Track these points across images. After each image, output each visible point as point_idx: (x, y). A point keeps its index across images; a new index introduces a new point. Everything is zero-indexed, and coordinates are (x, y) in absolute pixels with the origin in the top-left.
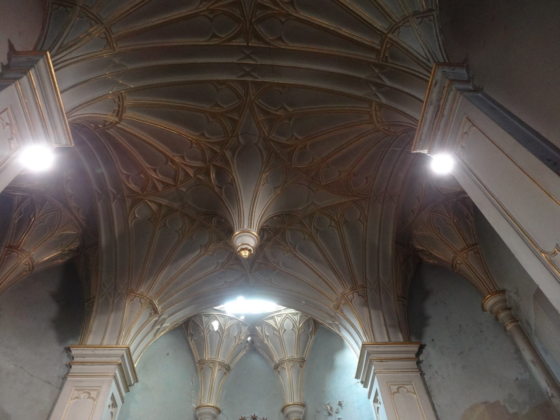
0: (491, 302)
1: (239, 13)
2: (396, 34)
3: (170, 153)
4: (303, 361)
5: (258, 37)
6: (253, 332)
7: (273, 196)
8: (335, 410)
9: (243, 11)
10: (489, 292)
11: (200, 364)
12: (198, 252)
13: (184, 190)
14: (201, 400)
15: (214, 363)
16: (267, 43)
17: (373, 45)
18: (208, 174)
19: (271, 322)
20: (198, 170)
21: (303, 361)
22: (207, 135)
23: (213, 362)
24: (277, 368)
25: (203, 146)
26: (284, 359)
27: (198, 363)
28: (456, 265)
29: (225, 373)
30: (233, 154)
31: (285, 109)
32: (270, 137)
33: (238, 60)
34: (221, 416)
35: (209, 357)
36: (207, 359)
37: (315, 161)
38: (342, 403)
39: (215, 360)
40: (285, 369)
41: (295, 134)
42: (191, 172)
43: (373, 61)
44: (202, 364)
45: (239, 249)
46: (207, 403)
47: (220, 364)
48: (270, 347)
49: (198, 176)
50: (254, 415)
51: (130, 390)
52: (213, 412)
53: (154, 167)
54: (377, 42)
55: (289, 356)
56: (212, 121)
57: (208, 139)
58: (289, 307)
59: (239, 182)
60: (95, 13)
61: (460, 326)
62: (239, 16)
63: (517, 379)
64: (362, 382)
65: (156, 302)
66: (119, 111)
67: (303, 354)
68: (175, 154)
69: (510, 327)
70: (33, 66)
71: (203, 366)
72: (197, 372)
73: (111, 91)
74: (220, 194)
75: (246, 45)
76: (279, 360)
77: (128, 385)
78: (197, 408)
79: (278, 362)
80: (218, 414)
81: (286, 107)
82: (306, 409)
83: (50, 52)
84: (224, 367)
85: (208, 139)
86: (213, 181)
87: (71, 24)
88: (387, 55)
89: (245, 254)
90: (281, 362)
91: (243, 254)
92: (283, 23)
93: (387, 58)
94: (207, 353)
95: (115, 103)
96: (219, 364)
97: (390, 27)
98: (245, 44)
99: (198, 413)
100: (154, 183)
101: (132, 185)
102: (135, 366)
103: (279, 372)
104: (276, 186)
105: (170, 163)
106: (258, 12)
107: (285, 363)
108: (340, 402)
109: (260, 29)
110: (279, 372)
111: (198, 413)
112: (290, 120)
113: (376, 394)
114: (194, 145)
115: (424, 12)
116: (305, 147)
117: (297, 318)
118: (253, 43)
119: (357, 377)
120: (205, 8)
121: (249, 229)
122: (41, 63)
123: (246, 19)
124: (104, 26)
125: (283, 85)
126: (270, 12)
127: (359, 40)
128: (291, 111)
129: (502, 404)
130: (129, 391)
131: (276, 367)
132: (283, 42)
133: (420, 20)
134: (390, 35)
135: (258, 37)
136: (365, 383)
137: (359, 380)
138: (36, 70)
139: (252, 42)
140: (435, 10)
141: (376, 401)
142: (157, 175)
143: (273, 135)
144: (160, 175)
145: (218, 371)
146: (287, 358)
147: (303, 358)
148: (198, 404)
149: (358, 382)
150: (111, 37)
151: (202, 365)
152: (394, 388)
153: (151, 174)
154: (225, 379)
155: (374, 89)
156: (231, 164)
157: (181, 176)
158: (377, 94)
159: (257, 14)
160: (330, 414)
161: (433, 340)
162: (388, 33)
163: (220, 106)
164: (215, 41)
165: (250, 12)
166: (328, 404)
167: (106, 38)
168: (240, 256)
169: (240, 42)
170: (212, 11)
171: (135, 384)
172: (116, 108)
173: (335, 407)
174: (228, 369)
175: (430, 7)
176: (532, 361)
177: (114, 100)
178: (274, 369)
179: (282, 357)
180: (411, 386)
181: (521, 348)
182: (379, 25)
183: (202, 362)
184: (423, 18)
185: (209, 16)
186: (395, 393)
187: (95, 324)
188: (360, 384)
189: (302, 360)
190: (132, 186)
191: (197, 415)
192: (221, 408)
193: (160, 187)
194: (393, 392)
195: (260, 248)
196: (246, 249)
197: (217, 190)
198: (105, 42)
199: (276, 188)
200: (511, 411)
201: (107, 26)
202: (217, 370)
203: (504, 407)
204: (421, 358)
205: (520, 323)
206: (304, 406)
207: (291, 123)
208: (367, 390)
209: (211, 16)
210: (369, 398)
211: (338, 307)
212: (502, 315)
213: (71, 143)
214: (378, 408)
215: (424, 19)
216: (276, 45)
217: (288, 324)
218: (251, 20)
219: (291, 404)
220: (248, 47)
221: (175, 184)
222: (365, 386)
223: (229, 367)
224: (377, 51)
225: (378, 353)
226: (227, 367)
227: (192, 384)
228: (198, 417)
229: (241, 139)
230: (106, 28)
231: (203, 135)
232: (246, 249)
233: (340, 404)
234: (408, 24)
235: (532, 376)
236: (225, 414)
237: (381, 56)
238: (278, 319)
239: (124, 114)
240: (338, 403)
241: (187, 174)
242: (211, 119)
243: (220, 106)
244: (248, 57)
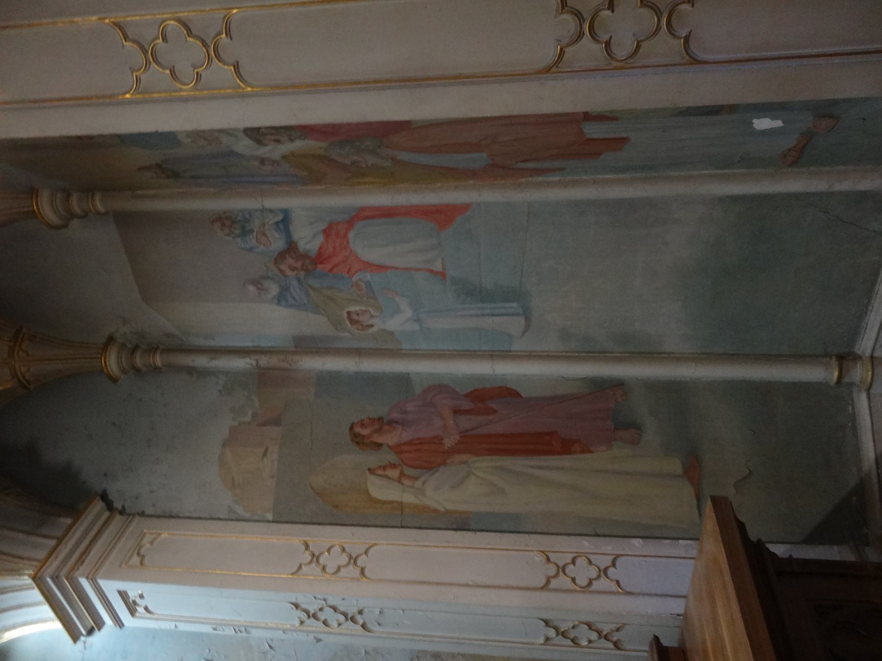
0: (112, 362)
10: (98, 358)
28: (24, 377)
61: (114, 424)
63: (220, 391)
69: (158, 361)
129: (236, 424)
152: (136, 560)
161: (105, 475)
176: (212, 359)
180: (147, 535)
181: (191, 364)
186: (142, 563)
194: (138, 563)
200: (248, 418)
203: (240, 424)
204: (118, 505)
205: (161, 347)
212: (139, 360)
214: (146, 609)
222: (99, 624)
225: (64, 563)
235: (227, 373)
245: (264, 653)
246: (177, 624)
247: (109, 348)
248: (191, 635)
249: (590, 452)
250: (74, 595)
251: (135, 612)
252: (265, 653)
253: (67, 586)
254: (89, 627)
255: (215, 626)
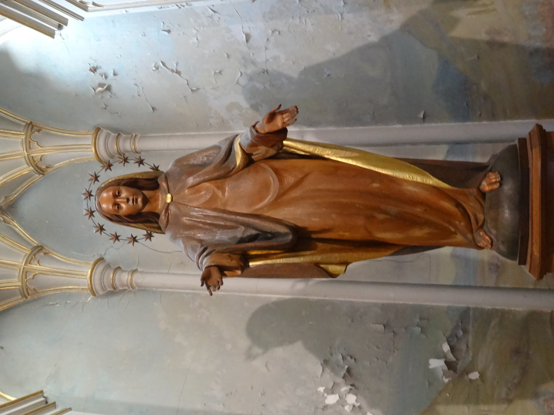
4: (31, 126)
8: (102, 80)
11: (28, 294)
14: (83, 289)
15: (27, 272)
21: (31, 127)
23: (25, 272)
24: (41, 169)
26: (26, 155)
27: (27, 298)
29: (45, 254)
34: (107, 258)
35: (16, 280)
36: (20, 284)
38: (93, 67)
39: (22, 270)
40: (42, 155)
44: (27, 290)
46: (86, 279)
47: (29, 261)
48: (5, 180)
50: (84, 194)
51: (53, 401)
52: (100, 268)
55: (21, 149)
64: (60, 27)
67: (20, 125)
71: (30, 289)
72: (39, 299)
76: (29, 165)
77: (44, 405)
78: (94, 294)
79: (31, 168)
80: (105, 261)
82: (104, 128)
84: (34, 255)
90: (31, 161)
94: (10, 284)
96: (30, 263)
99: (101, 293)
102: (13, 399)
103: (47, 167)
107: (32, 155)
108: (91, 70)
110: (47, 167)
111: (101, 293)
119: (51, 34)
130: (54, 403)
131: (41, 171)
137: (57, 32)
145: (40, 265)
146: (25, 152)
147: (26, 125)
148: (89, 293)
149: (61, 35)
151: (29, 290)
154: (55, 253)
160: (109, 89)
166: (95, 90)
171: (45, 395)
173: (97, 78)
174: (39, 248)
178: (44, 175)
179: (23, 160)
183: (25, 292)
187: (452, 360)
188: (62, 31)
189: (28, 127)
191: (104, 293)
192: (97, 257)
202: (38, 266)
206: (98, 130)
208: (71, 19)
210: (82, 19)
214: (94, 4)
219: (93, 149)
222: (65, 22)
223: (38, 247)
226: (36, 251)
227: (58, 305)
228: (106, 291)
233: (93, 69)
236: (105, 252)
240: (92, 73)
245: (210, 17)
246: (127, 10)
247: (100, 262)
248: (143, 15)
249: (164, 233)
250: (31, 9)
251: (87, 8)
252: (211, 17)
253: (18, 4)
254: (58, 25)
255: (160, 6)
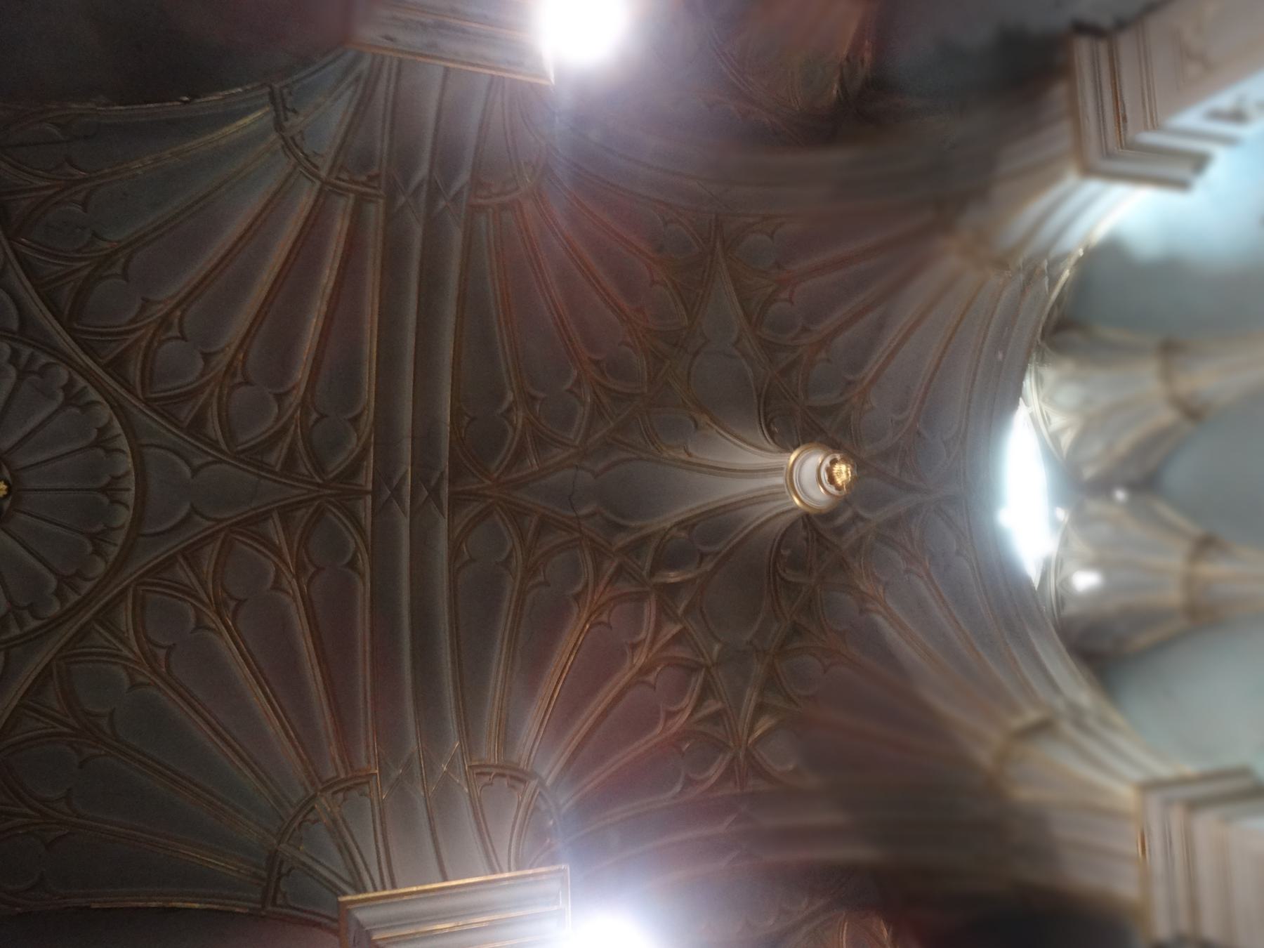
1: (304, 510)
2: (318, 161)
3: (623, 676)
5: (354, 470)
6: (1101, 487)
7: (717, 431)
9: (300, 502)
12: (879, 619)
13: (717, 647)
16: (365, 450)
17: (349, 210)
18: (673, 589)
19: (1067, 440)
20: (664, 612)
22: (579, 588)
23: (1189, 582)
25: (604, 599)
30: (620, 528)
31: (509, 410)
32: (577, 443)
33: (406, 516)
37: (629, 339)
41: (568, 385)
42: (672, 629)
43: (381, 209)
45: (832, 489)
49: (680, 611)
53: (662, 715)
54: (342, 202)
56: (545, 576)
57: (586, 585)
58: (1018, 392)
59: (682, 511)
60: (292, 811)
62: (311, 510)
65: (1016, 723)
66: (512, 777)
68: (628, 664)
70: (368, 933)
73: (463, 788)
74: (720, 556)
75: (370, 497)
81: (505, 405)
83: (345, 894)
85: (586, 585)
86: (689, 576)
87: (309, 862)
88: (364, 178)
89: (843, 472)
91: (844, 477)
92: (322, 416)
93: (371, 178)
95: (492, 784)
97: (307, 177)
98: (369, 498)
100: (700, 721)
101: (712, 771)
104: (693, 426)
105: (651, 678)
106: (304, 471)
109: (338, 463)
112: (534, 398)
113: (1216, 115)
114: (604, 618)
115: (276, 110)
116: (596, 363)
117: (1049, 374)
118: (366, 480)
119: (1182, 185)
120: (294, 582)
121: (784, 472)
122: (363, 915)
123: (314, 495)
124: (319, 793)
125: (456, 414)
126: (300, 444)
127: (342, 244)
128: (514, 396)
132: (361, 414)
133: (290, 114)
134: (323, 174)
135: (354, 470)
136: (1199, 162)
138: (375, 930)
139: (363, 484)
140: (271, 87)
141: (1237, 116)
142: (682, 710)
143: (572, 437)
144: (683, 704)
150: (346, 780)
153: (678, 725)
155: (442, 203)
156: (644, 532)
157: (680, 652)
158: (452, 193)
159: (307, 473)
162: (319, 178)
163: (510, 556)
164: (364, 563)
165: (302, 488)
167: (349, 789)
168: (849, 486)
169: (365, 508)
170: (300, 568)
172: (505, 781)
175: (266, 99)
177: (486, 784)
182: (304, 200)
184: (285, 108)
185: (310, 573)
190: (714, 773)
193: (712, 706)
195: (832, 445)
196: (829, 471)
197: (708, 566)
198: (355, 793)
199: (696, 426)
201: (320, 787)
204: (1105, 21)
207: (541, 395)
209: (312, 570)
211: (1001, 264)
213: (559, 871)
215: (288, 106)
216: (368, 429)
217: (1070, 394)
218: (318, 485)
220: (375, 494)
221: (704, 669)
224: (362, 199)
229: (584, 511)
230: (324, 790)
231: (577, 597)
232: (829, 471)
234: (298, 138)
237: (368, 190)
238: (1058, 421)
239: (521, 766)
241: (677, 639)
242: (541, 578)
243: (510, 556)
244: (397, 491)
